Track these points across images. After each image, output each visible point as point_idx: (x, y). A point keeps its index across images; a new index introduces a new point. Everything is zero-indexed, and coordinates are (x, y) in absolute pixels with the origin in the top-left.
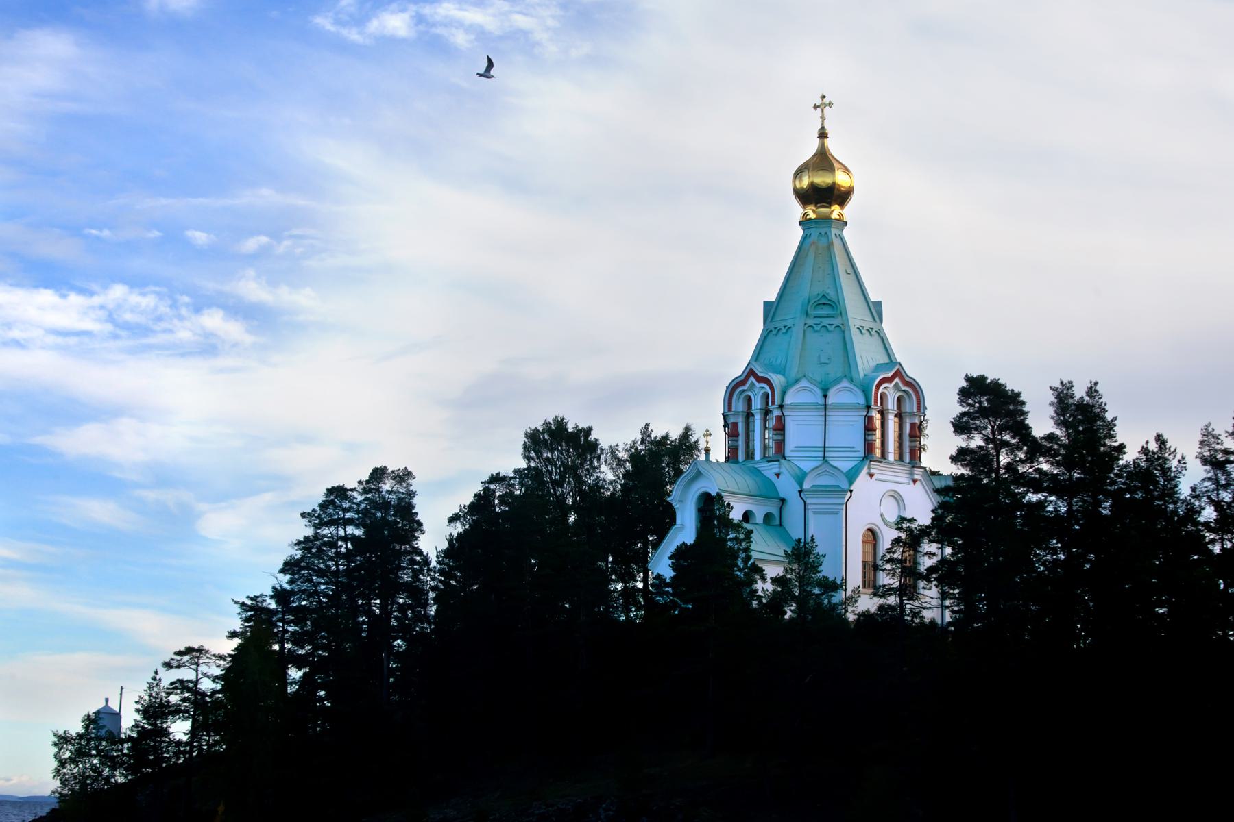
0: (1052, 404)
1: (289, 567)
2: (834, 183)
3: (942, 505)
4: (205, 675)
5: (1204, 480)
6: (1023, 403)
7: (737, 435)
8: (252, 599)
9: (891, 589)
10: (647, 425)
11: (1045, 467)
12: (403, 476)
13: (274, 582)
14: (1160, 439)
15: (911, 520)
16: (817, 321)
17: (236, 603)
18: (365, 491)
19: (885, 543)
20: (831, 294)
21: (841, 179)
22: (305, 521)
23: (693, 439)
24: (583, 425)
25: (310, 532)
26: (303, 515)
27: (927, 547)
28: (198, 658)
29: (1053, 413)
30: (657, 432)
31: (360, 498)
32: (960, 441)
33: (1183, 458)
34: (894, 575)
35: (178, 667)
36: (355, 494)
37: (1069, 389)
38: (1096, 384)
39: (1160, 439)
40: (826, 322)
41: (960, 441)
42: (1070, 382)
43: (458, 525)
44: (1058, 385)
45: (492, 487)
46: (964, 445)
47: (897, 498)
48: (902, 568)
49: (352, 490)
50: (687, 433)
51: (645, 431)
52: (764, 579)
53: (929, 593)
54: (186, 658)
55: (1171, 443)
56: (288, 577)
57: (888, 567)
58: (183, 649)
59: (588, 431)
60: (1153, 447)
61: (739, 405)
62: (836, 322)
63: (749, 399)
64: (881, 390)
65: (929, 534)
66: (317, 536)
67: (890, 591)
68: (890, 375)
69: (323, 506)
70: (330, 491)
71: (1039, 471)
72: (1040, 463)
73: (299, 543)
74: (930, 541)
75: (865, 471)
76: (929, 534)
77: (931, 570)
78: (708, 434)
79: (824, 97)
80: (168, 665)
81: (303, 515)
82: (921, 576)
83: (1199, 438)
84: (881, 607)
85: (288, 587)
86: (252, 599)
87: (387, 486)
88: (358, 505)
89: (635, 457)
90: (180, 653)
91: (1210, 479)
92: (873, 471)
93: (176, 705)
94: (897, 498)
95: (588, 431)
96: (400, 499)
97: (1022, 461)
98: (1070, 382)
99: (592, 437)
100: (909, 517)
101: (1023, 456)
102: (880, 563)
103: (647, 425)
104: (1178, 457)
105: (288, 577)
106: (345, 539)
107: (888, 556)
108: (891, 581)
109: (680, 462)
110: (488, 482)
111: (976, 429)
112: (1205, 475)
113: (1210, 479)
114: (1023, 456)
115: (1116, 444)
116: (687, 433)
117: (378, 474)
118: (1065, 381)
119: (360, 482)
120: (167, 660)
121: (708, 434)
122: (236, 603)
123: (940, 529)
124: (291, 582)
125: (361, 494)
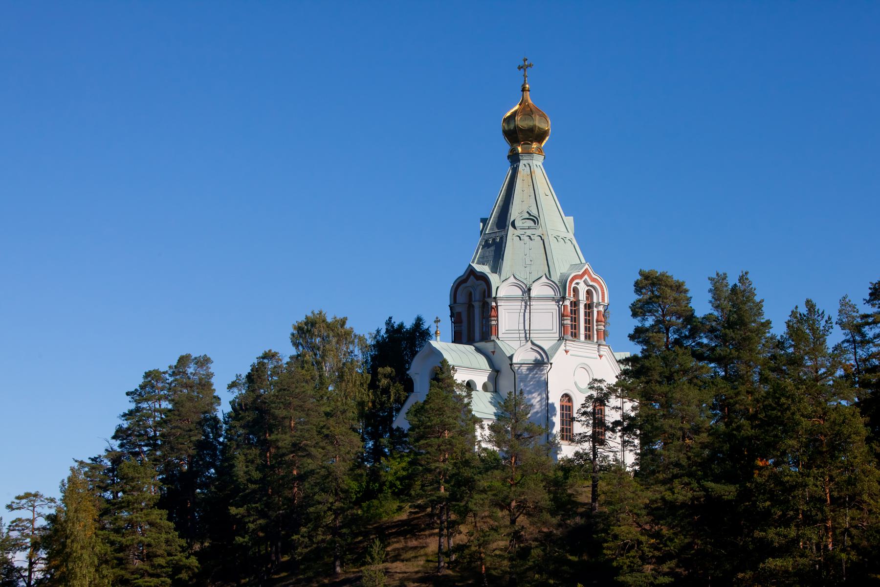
0: (710, 291)
1: (119, 434)
2: (535, 126)
3: (625, 372)
4: (40, 515)
5: (843, 342)
6: (686, 291)
7: (461, 322)
8: (92, 460)
9: (585, 436)
10: (390, 318)
11: (705, 341)
12: (204, 362)
13: (106, 445)
14: (810, 305)
15: (600, 381)
16: (522, 232)
17: (76, 461)
18: (174, 374)
19: (577, 404)
20: (534, 212)
21: (540, 123)
22: (129, 398)
23: (425, 326)
24: (340, 316)
25: (133, 406)
26: (128, 394)
27: (614, 401)
28: (34, 501)
29: (711, 299)
30: (396, 322)
31: (171, 379)
32: (636, 322)
33: (830, 318)
34: (587, 425)
35: (19, 508)
36: (167, 376)
37: (724, 279)
38: (746, 273)
39: (810, 305)
40: (529, 232)
41: (636, 322)
42: (725, 274)
43: (235, 390)
44: (714, 276)
45: (266, 361)
46: (640, 325)
47: (586, 368)
48: (594, 419)
49: (164, 373)
50: (419, 321)
51: (389, 322)
52: (482, 428)
53: (614, 440)
54: (24, 501)
55: (819, 307)
56: (119, 442)
57: (583, 418)
58: (22, 494)
59: (343, 322)
60: (803, 310)
61: (461, 299)
62: (538, 232)
63: (470, 294)
64: (573, 285)
65: (615, 391)
66: (138, 409)
67: (583, 438)
68: (580, 273)
69: (142, 387)
70: (147, 375)
71: (700, 344)
72: (701, 338)
73: (125, 415)
74: (617, 397)
75: (562, 347)
76: (615, 391)
77: (616, 423)
78: (437, 321)
79: (525, 60)
80: (10, 507)
81: (128, 394)
82: (607, 429)
83: (838, 307)
84: (577, 454)
85: (119, 450)
86: (92, 460)
87: (190, 370)
88: (170, 384)
89: (380, 345)
90: (18, 498)
91: (848, 341)
92: (568, 348)
93: (17, 539)
94: (586, 368)
95: (343, 322)
96: (201, 379)
97: (686, 337)
98: (725, 274)
99: (347, 326)
100: (599, 378)
101: (687, 333)
102: (575, 415)
103: (390, 318)
104: (826, 318)
105: (119, 442)
106: (161, 411)
107: (583, 410)
108: (586, 430)
109: (415, 346)
110: (263, 358)
111: (650, 311)
112: (844, 338)
113: (848, 341)
114: (687, 333)
115: (763, 321)
116: (419, 321)
117: (183, 360)
118: (721, 273)
119: (170, 367)
120: (9, 503)
121: (437, 321)
122: (76, 461)
123: (624, 388)
124: (121, 446)
125: (171, 376)
